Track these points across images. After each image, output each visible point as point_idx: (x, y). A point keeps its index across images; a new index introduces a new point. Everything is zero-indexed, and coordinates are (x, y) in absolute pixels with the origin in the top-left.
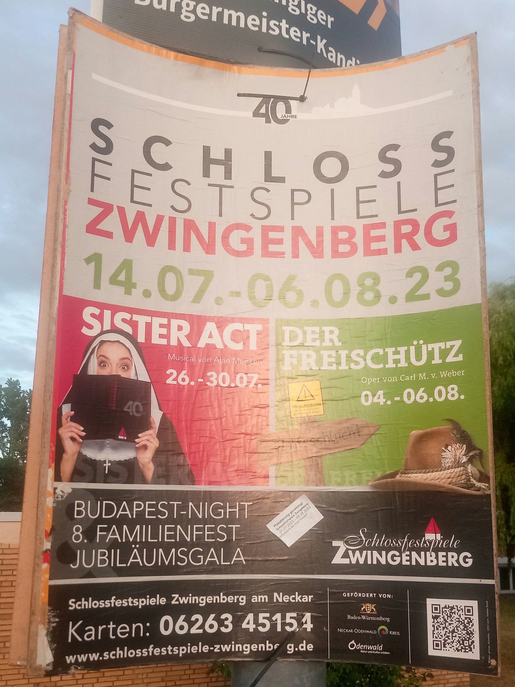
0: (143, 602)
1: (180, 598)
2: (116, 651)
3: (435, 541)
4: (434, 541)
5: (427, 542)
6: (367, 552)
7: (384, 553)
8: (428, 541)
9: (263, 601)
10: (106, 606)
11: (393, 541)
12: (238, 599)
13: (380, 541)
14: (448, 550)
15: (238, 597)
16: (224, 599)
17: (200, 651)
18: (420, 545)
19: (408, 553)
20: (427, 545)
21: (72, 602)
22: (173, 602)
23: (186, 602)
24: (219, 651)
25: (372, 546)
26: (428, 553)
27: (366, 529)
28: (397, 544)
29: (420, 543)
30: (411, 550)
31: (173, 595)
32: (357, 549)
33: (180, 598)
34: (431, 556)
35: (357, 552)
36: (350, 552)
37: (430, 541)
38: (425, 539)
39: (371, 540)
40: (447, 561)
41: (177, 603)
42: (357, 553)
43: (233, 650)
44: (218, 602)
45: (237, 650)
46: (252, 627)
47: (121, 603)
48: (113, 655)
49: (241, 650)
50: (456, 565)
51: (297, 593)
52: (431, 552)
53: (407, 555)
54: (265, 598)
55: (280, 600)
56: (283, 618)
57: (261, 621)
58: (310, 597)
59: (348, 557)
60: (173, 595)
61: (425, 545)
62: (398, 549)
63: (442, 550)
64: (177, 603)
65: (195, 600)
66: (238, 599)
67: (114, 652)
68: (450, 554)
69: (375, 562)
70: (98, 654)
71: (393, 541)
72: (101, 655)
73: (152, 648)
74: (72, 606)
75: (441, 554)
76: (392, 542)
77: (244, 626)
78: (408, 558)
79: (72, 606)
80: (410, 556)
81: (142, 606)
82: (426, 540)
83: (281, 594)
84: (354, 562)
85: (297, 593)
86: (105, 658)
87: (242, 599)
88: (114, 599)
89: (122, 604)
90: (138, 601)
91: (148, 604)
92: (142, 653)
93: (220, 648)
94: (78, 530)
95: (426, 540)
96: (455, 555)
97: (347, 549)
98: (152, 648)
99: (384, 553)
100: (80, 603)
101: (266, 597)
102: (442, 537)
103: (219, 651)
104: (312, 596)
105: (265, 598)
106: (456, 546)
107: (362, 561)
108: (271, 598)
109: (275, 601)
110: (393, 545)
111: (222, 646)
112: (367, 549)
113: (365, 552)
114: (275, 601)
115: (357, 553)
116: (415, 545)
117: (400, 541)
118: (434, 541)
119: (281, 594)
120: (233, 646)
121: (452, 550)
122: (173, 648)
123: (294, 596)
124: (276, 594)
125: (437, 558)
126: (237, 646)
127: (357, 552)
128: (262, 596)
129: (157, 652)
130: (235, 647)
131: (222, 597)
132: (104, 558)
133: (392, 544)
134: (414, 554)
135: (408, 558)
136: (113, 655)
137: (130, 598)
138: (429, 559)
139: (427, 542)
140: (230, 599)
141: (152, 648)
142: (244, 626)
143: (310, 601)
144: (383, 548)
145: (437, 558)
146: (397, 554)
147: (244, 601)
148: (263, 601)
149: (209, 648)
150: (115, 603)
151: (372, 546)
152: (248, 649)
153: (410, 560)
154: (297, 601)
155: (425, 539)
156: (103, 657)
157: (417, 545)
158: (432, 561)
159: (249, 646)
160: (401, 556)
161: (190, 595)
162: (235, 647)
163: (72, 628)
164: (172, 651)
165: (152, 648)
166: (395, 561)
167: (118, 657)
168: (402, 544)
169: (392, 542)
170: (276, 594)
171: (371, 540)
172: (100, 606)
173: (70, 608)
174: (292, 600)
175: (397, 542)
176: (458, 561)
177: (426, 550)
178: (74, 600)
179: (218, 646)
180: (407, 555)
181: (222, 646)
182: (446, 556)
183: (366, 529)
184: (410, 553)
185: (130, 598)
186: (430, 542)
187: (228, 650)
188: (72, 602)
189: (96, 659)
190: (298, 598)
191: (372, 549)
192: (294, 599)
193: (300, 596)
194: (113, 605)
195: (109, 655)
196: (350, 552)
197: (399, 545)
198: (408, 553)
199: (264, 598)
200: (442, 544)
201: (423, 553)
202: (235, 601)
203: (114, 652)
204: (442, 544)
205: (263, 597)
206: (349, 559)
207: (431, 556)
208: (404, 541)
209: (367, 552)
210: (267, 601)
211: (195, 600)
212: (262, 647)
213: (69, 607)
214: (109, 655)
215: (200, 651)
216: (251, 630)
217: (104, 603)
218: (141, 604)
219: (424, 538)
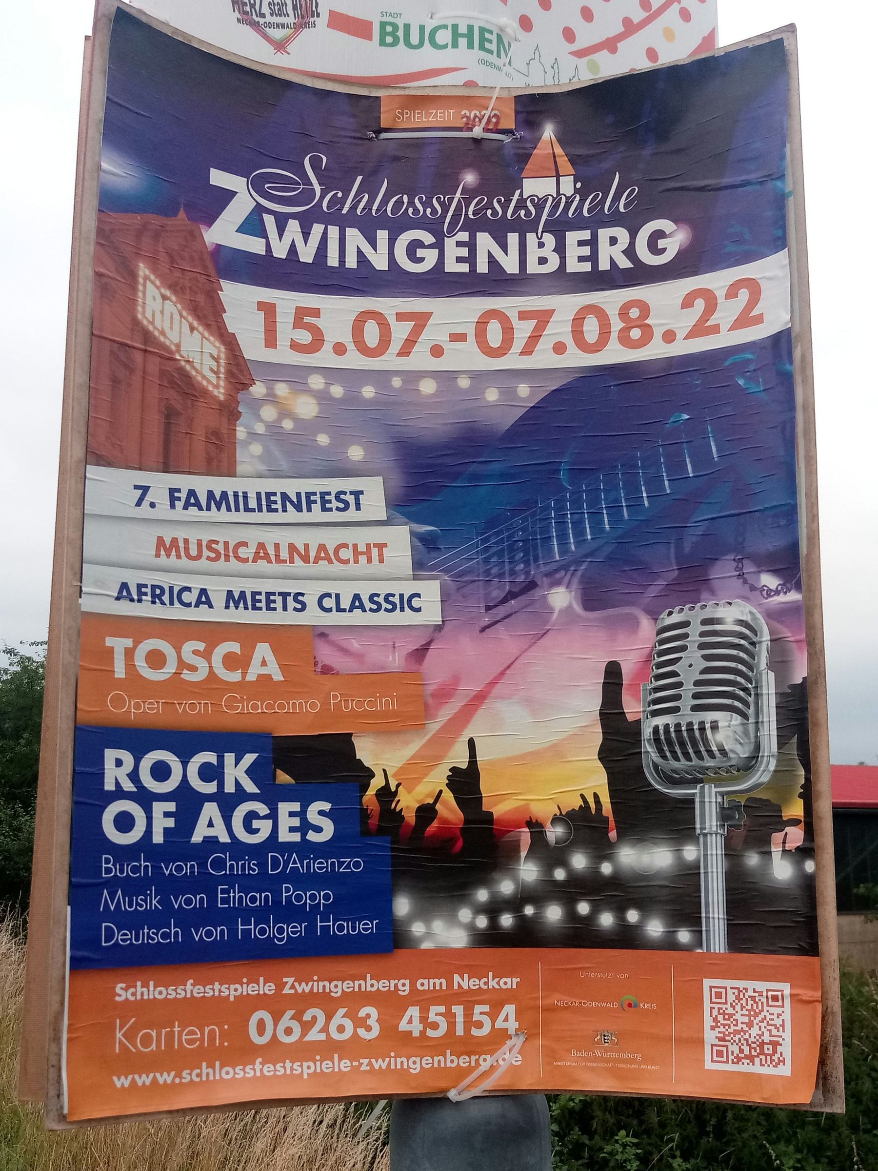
0: (236, 990)
1: (296, 984)
2: (201, 1070)
3: (554, 199)
4: (550, 198)
5: (529, 204)
6: (326, 229)
7: (382, 235)
8: (532, 201)
9: (438, 988)
10: (178, 996)
11: (416, 201)
12: (396, 985)
13: (370, 202)
14: (597, 221)
15: (396, 981)
16: (372, 985)
17: (336, 1070)
18: (505, 212)
19: (464, 236)
20: (528, 213)
21: (122, 988)
22: (287, 991)
23: (307, 990)
24: (368, 1068)
25: (344, 211)
26: (531, 238)
27: (325, 159)
28: (429, 210)
29: (505, 209)
30: (473, 227)
31: (285, 980)
32: (294, 216)
33: (296, 984)
34: (541, 245)
35: (293, 226)
36: (269, 221)
37: (539, 199)
38: (521, 194)
39: (340, 195)
40: (593, 258)
41: (293, 991)
42: (293, 227)
43: (393, 1067)
44: (363, 989)
45: (399, 1067)
46: (416, 1028)
47: (203, 991)
48: (198, 1075)
49: (405, 1067)
50: (624, 263)
51: (491, 974)
52: (542, 232)
53: (459, 244)
54: (441, 984)
55: (465, 986)
56: (468, 1014)
57: (432, 1017)
58: (515, 980)
59: (263, 234)
60: (285, 980)
61: (523, 213)
62: (435, 227)
63: (578, 224)
64: (293, 991)
65: (324, 986)
66: (396, 985)
67: (198, 1071)
68: (604, 234)
69: (351, 262)
70: (173, 1074)
71: (416, 201)
72: (179, 1075)
73: (260, 1064)
74: (120, 995)
75: (572, 237)
76: (411, 203)
77: (403, 1026)
78: (464, 252)
79: (120, 995)
80: (471, 245)
81: (235, 996)
82: (525, 197)
83: (466, 976)
84: (280, 251)
85: (491, 974)
86: (183, 1080)
87: (404, 985)
88: (192, 985)
89: (205, 992)
90: (229, 989)
91: (245, 993)
92: (245, 1073)
93: (370, 1064)
94: (107, 861)
95: (525, 197)
96: (622, 234)
97: (259, 210)
98: (261, 1063)
99: (382, 235)
100: (133, 990)
101: (443, 981)
102: (579, 185)
103: (368, 1068)
104: (518, 980)
105: (441, 984)
106: (625, 207)
107: (307, 255)
108: (450, 983)
109: (456, 987)
110: (417, 210)
111: (373, 1061)
112: (327, 220)
113: (317, 229)
114: (456, 987)
115: (293, 227)
116: (489, 212)
117: (438, 199)
118: (550, 198)
119: (466, 976)
120: (393, 1060)
121: (615, 220)
122: (293, 1065)
123: (486, 980)
124: (457, 978)
125: (560, 249)
126: (399, 1060)
127: (293, 226)
128: (436, 980)
129: (268, 1071)
130: (396, 1061)
131: (369, 982)
132: (110, 866)
133: (410, 210)
134: (485, 241)
135: (464, 252)
136: (198, 1075)
137: (217, 984)
138: (533, 253)
139: (529, 204)
140: (383, 985)
141: (260, 1064)
142: (403, 1026)
143: (514, 987)
144: (382, 222)
145: (560, 249)
146: (428, 238)
147: (407, 988)
148: (438, 988)
149: (352, 1064)
150: (192, 991)
151: (344, 211)
152: (418, 1066)
153: (471, 259)
154: (491, 987)
155: (521, 194)
156: (181, 1078)
157: (495, 213)
158: (543, 261)
159: (418, 1060)
160: (439, 245)
161: (315, 978)
162: (396, 1061)
163: (120, 1031)
164: (292, 1069)
165: (261, 1063)
166: (422, 260)
167: (204, 1078)
168: (445, 210)
169: (411, 203)
170: (457, 978)
171: (340, 195)
172: (169, 997)
173: (117, 998)
174: (482, 986)
175: (427, 204)
176: (630, 252)
177: (524, 227)
178: (123, 985)
179: (366, 1061)
180: (459, 244)
181: (373, 1061)
182: (593, 243)
183: (325, 159)
184: (473, 238)
185: (217, 984)
186: (540, 205)
187: (384, 1067)
188: (122, 988)
189: (169, 1081)
190: (493, 983)
191: (343, 223)
192: (486, 983)
193: (497, 980)
194: (189, 996)
195: (190, 1074)
196: (269, 221)
197: (434, 211)
198: (464, 236)
199: (440, 983)
200: (580, 207)
201: (513, 239)
202: (392, 989)
203: (198, 1071)
204: (580, 207)
205: (437, 981)
206: (264, 240)
207: (541, 245)
208: (451, 200)
209: (326, 229)
210: (444, 987)
211: (324, 986)
212: (439, 1061)
213: (115, 997)
214: (190, 1074)
215: (336, 1070)
216: (416, 1034)
217: (175, 990)
218: (233, 993)
219: (518, 192)
